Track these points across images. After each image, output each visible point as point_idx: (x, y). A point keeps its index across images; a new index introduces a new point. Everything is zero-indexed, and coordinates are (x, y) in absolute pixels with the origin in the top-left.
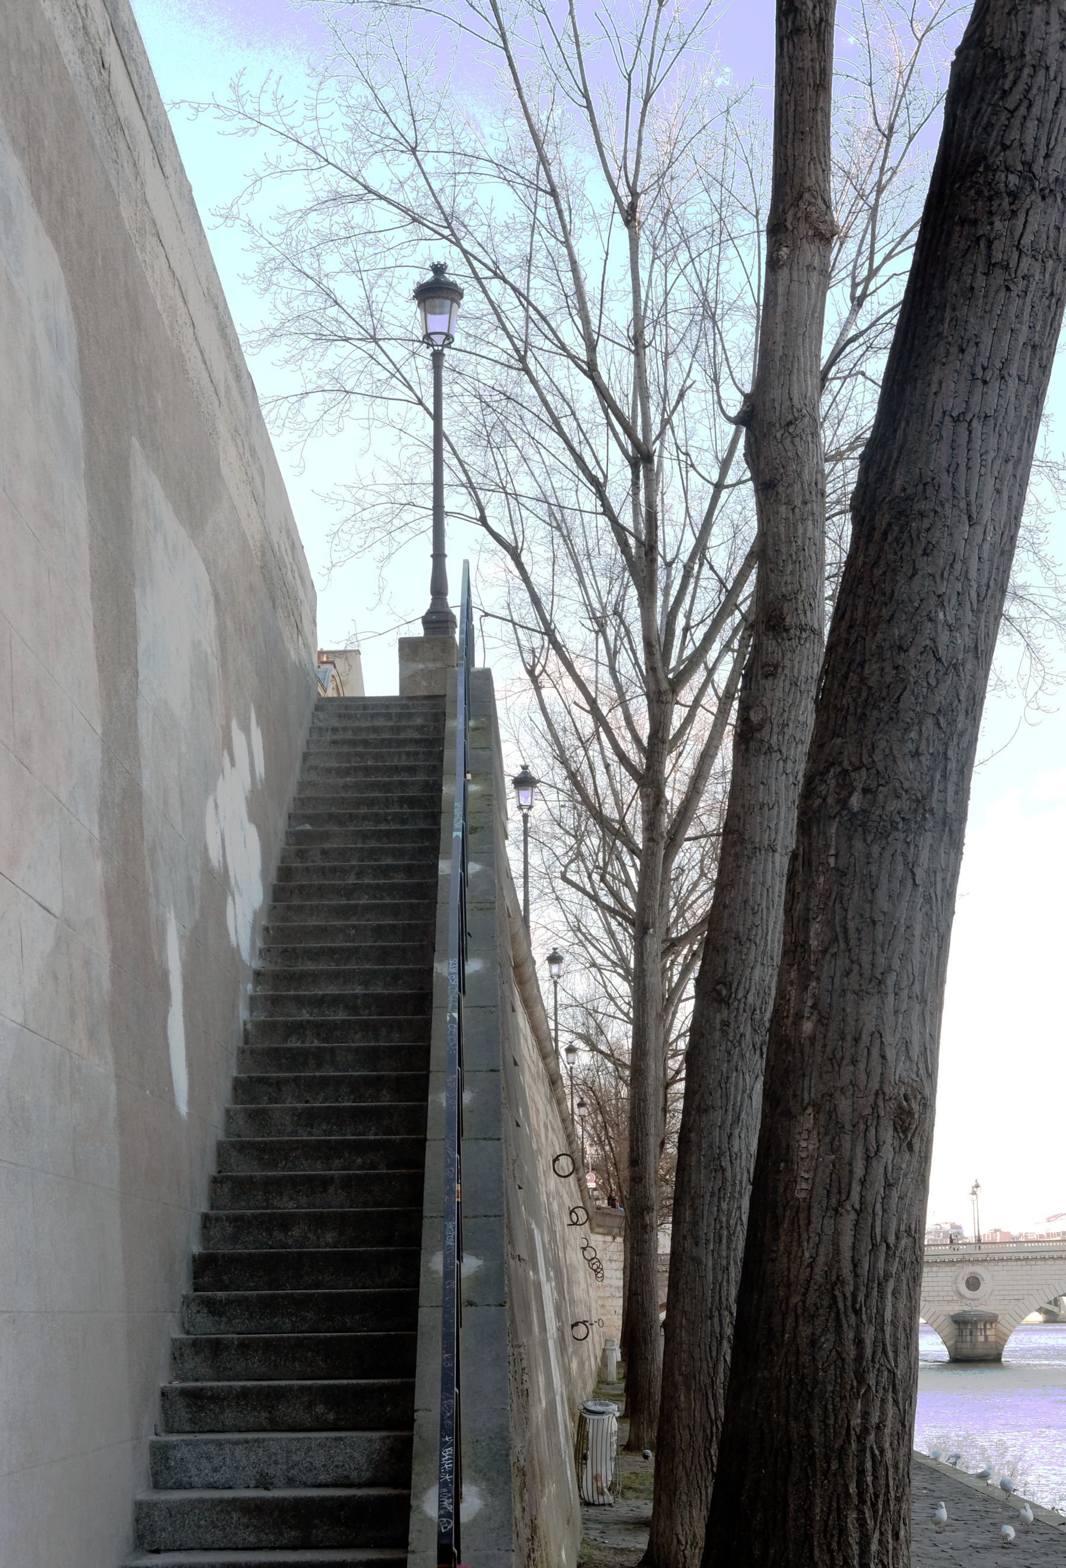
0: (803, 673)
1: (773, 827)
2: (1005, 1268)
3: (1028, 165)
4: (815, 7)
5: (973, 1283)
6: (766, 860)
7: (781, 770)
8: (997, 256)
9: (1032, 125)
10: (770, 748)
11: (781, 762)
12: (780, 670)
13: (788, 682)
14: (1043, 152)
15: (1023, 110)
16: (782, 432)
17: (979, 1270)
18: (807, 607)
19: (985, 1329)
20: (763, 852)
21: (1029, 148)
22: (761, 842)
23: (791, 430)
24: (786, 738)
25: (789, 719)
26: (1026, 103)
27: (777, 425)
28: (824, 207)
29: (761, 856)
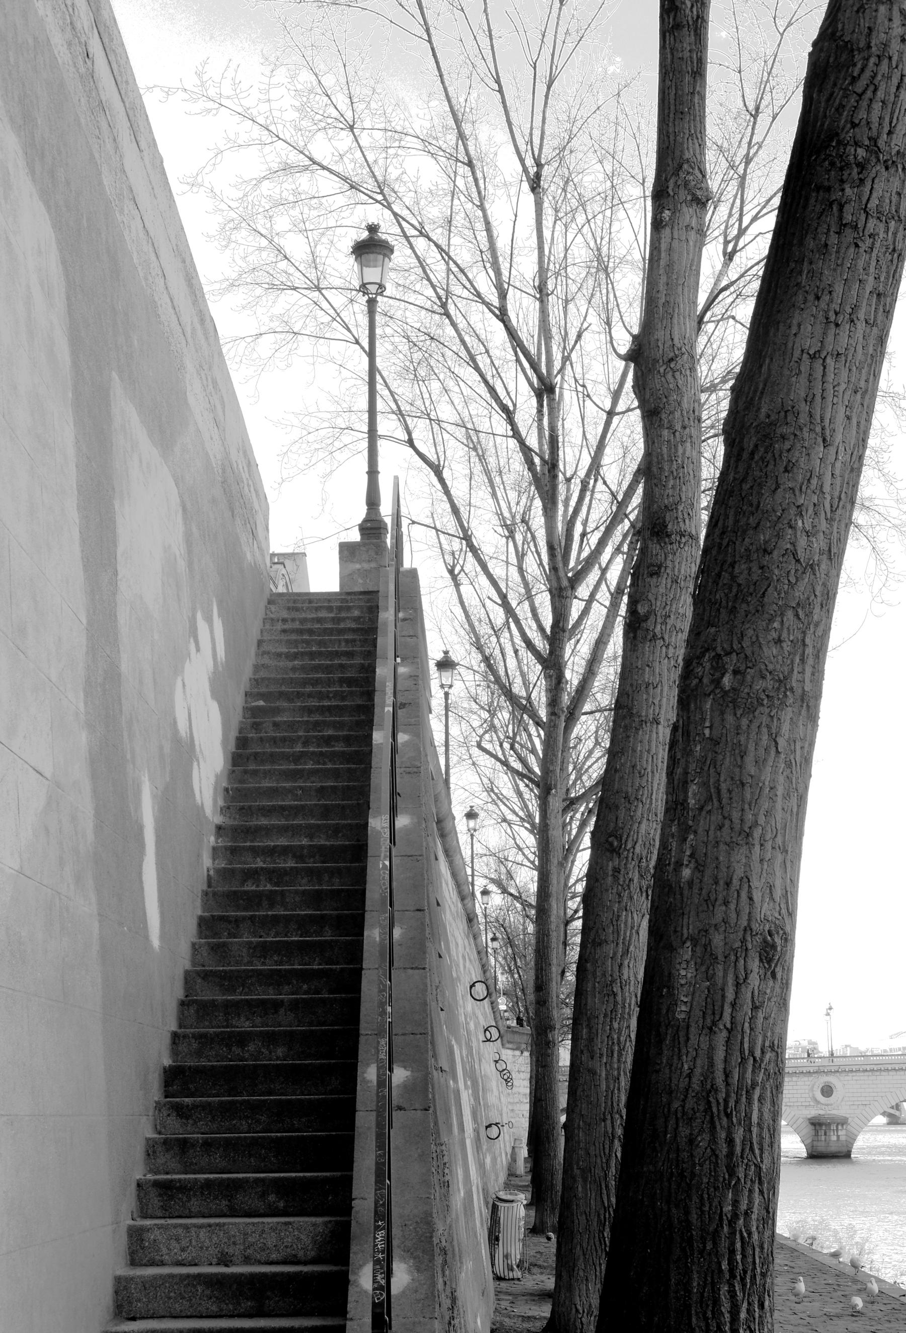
0: (683, 572)
1: (657, 702)
2: (855, 1078)
3: (874, 140)
4: (692, 6)
5: (827, 1091)
6: (651, 731)
7: (664, 655)
8: (848, 218)
10: (654, 635)
11: (664, 648)
12: (663, 569)
13: (669, 581)
14: (886, 129)
15: (869, 94)
16: (664, 367)
17: (832, 1079)
18: (686, 516)
19: (837, 1129)
20: (648, 724)
21: (875, 126)
22: (647, 716)
23: (672, 365)
24: (668, 627)
25: (670, 611)
26: (872, 88)
27: (661, 361)
28: (700, 176)
29: (647, 728)
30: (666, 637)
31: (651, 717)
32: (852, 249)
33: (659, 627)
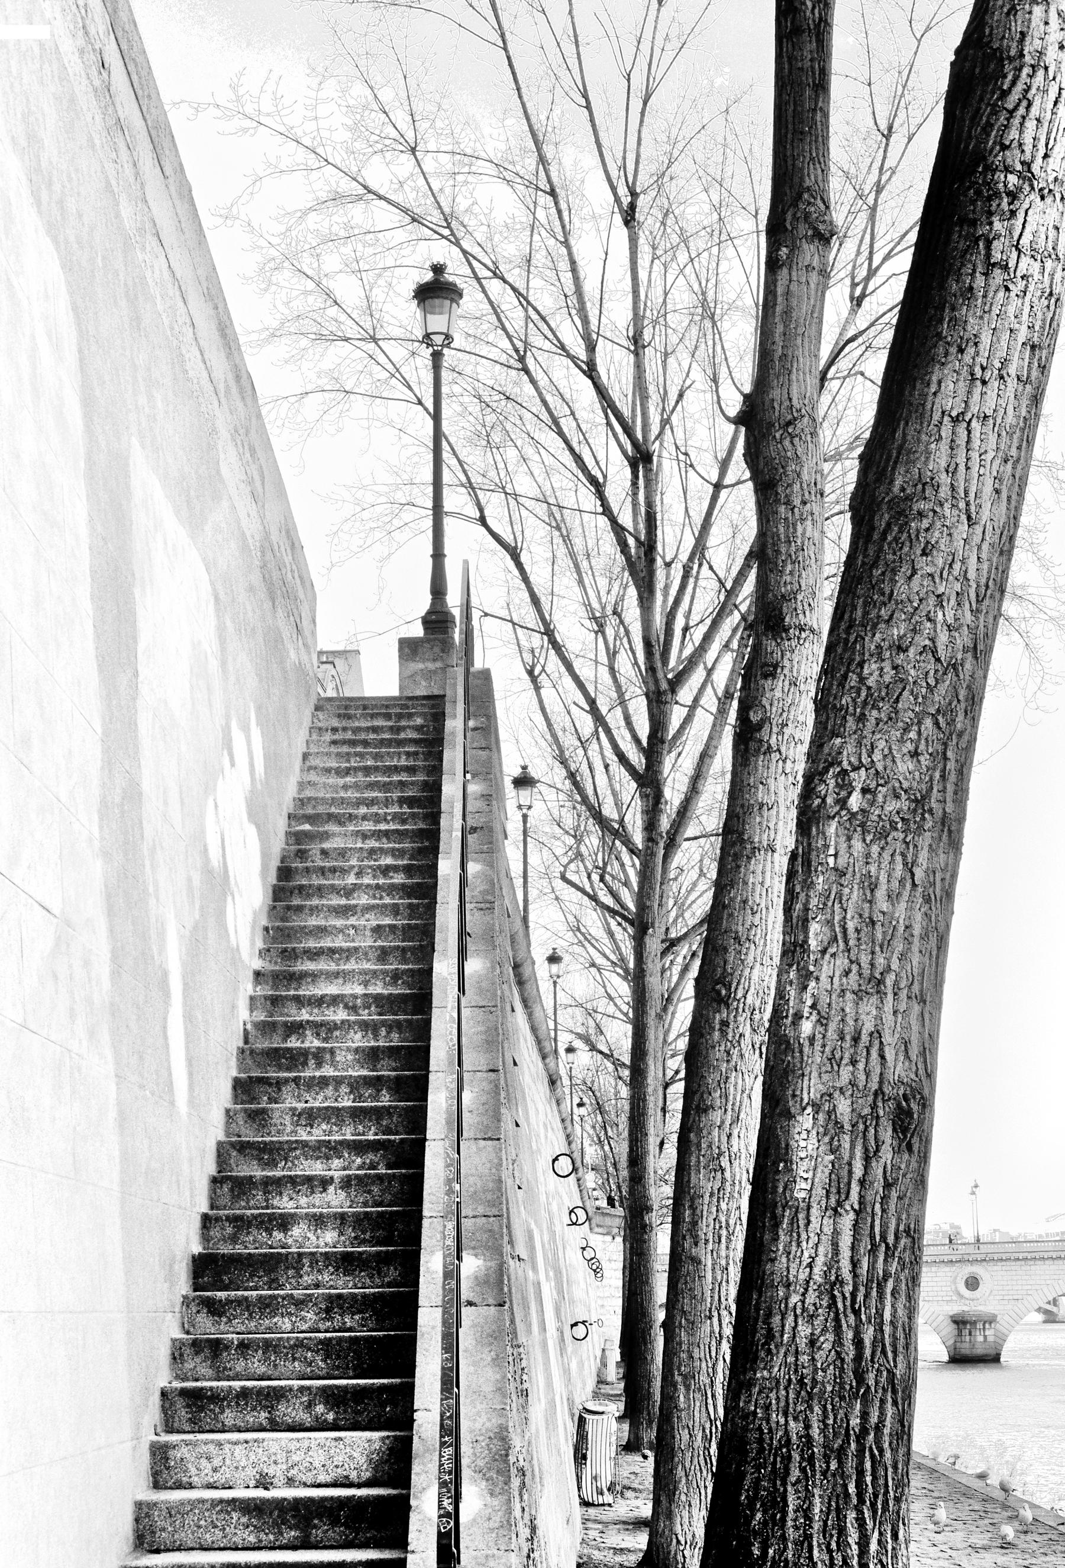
0: (802, 673)
1: (772, 826)
3: (1027, 165)
5: (972, 1283)
7: (780, 770)
8: (996, 256)
9: (1030, 125)
10: (769, 747)
13: (787, 683)
14: (1042, 151)
15: (1022, 111)
18: (806, 607)
21: (1028, 148)
26: (1024, 103)
28: (822, 207)
30: (783, 749)
31: (765, 844)
32: (1001, 294)
33: (774, 736)
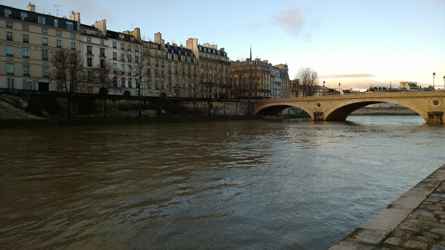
5: (319, 105)
